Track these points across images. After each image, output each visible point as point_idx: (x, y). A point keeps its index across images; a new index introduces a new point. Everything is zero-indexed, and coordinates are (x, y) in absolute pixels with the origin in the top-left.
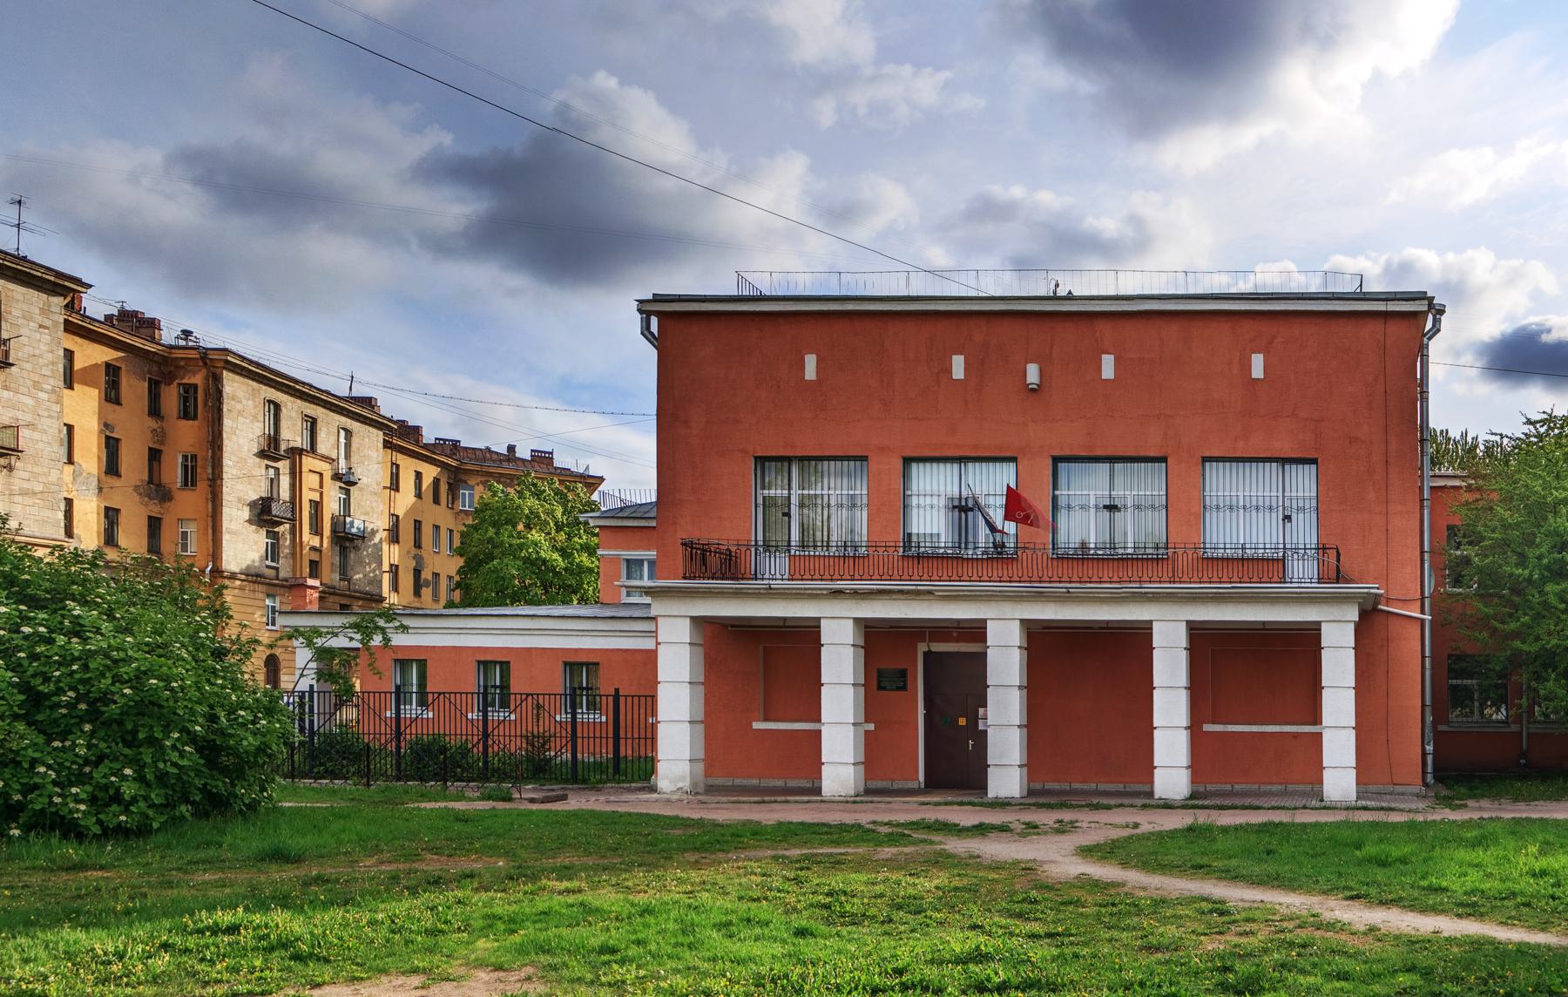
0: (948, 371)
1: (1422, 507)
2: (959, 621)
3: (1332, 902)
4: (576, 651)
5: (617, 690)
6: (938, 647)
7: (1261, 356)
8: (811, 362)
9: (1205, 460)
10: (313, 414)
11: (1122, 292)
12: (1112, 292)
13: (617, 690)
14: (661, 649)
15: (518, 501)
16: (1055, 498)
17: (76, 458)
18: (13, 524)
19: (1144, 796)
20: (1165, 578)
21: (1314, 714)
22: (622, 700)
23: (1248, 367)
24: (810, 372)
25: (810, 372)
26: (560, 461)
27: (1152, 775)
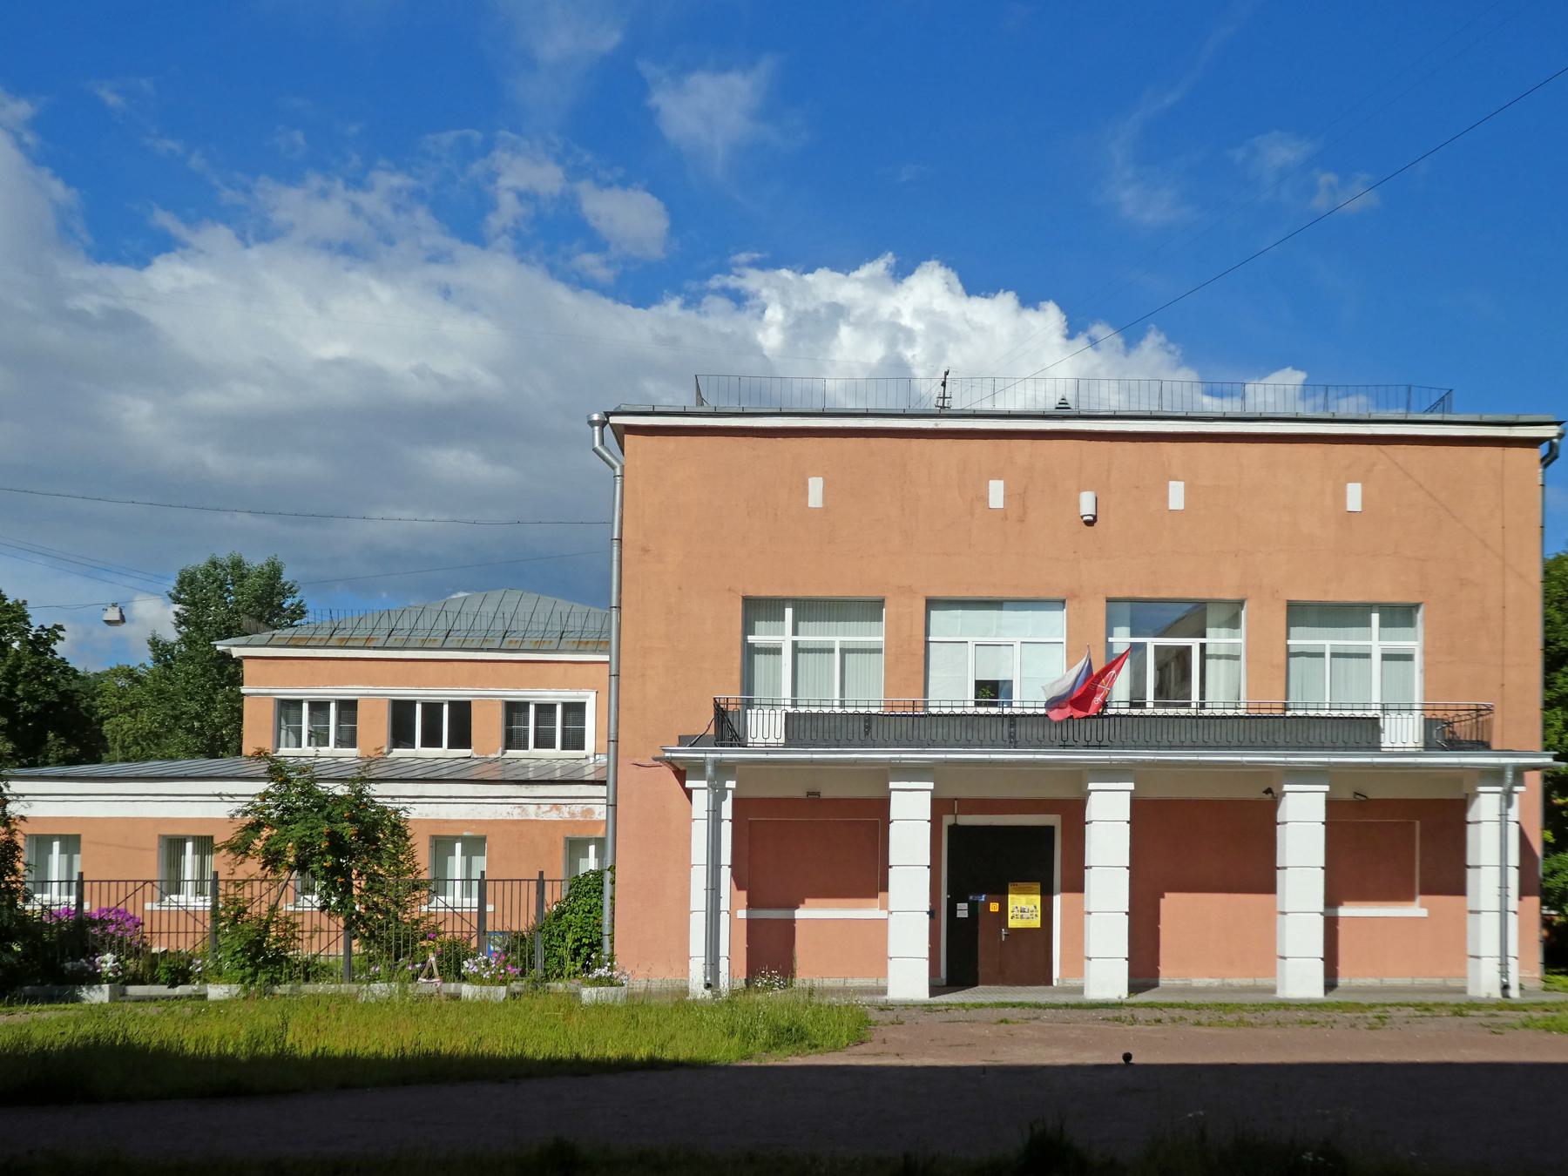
0: (985, 499)
1: (620, 600)
2: (912, 1069)
3: (730, 825)
4: (822, 907)
5: (541, 874)
6: (966, 820)
7: (1001, 483)
8: (816, 486)
9: (932, 604)
10: (269, 712)
11: (1319, 951)
12: (1319, 967)
13: (541, 874)
14: (893, 920)
15: (566, 954)
16: (1348, 614)
17: (1062, 597)
18: (408, 1052)
19: (1188, 705)
20: (381, 636)
21: (583, 723)
22: (87, 885)
23: (1341, 496)
24: (815, 497)
25: (815, 497)
26: (827, 793)
27: (886, 965)
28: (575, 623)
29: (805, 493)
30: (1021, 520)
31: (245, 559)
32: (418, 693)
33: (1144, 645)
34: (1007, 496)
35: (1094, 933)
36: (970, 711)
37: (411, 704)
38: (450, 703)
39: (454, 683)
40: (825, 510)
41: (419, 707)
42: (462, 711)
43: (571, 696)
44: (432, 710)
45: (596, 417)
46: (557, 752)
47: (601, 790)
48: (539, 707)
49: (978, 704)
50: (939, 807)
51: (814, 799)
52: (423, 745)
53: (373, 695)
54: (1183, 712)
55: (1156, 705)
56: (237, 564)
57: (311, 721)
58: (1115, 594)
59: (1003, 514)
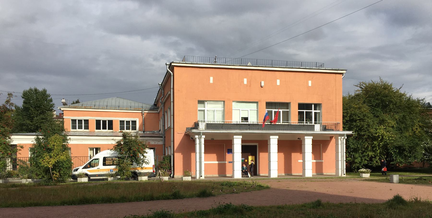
24: (211, 81)
25: (211, 81)
28: (101, 104)
29: (209, 80)
30: (250, 86)
31: (38, 88)
32: (102, 119)
33: (272, 111)
34: (247, 82)
35: (273, 164)
36: (241, 123)
37: (100, 121)
38: (103, 121)
39: (109, 117)
40: (213, 83)
41: (101, 121)
42: (111, 122)
43: (133, 119)
44: (104, 122)
45: (168, 63)
46: (83, 130)
47: (162, 139)
48: (78, 120)
49: (299, 123)
50: (243, 141)
51: (213, 139)
52: (126, 129)
53: (92, 119)
54: (280, 123)
55: (283, 122)
56: (36, 90)
57: (85, 124)
58: (200, 99)
59: (247, 85)
